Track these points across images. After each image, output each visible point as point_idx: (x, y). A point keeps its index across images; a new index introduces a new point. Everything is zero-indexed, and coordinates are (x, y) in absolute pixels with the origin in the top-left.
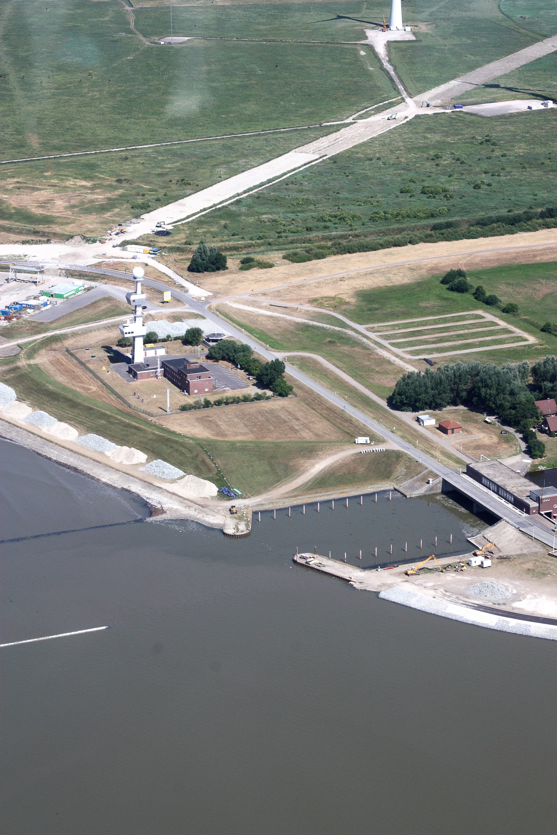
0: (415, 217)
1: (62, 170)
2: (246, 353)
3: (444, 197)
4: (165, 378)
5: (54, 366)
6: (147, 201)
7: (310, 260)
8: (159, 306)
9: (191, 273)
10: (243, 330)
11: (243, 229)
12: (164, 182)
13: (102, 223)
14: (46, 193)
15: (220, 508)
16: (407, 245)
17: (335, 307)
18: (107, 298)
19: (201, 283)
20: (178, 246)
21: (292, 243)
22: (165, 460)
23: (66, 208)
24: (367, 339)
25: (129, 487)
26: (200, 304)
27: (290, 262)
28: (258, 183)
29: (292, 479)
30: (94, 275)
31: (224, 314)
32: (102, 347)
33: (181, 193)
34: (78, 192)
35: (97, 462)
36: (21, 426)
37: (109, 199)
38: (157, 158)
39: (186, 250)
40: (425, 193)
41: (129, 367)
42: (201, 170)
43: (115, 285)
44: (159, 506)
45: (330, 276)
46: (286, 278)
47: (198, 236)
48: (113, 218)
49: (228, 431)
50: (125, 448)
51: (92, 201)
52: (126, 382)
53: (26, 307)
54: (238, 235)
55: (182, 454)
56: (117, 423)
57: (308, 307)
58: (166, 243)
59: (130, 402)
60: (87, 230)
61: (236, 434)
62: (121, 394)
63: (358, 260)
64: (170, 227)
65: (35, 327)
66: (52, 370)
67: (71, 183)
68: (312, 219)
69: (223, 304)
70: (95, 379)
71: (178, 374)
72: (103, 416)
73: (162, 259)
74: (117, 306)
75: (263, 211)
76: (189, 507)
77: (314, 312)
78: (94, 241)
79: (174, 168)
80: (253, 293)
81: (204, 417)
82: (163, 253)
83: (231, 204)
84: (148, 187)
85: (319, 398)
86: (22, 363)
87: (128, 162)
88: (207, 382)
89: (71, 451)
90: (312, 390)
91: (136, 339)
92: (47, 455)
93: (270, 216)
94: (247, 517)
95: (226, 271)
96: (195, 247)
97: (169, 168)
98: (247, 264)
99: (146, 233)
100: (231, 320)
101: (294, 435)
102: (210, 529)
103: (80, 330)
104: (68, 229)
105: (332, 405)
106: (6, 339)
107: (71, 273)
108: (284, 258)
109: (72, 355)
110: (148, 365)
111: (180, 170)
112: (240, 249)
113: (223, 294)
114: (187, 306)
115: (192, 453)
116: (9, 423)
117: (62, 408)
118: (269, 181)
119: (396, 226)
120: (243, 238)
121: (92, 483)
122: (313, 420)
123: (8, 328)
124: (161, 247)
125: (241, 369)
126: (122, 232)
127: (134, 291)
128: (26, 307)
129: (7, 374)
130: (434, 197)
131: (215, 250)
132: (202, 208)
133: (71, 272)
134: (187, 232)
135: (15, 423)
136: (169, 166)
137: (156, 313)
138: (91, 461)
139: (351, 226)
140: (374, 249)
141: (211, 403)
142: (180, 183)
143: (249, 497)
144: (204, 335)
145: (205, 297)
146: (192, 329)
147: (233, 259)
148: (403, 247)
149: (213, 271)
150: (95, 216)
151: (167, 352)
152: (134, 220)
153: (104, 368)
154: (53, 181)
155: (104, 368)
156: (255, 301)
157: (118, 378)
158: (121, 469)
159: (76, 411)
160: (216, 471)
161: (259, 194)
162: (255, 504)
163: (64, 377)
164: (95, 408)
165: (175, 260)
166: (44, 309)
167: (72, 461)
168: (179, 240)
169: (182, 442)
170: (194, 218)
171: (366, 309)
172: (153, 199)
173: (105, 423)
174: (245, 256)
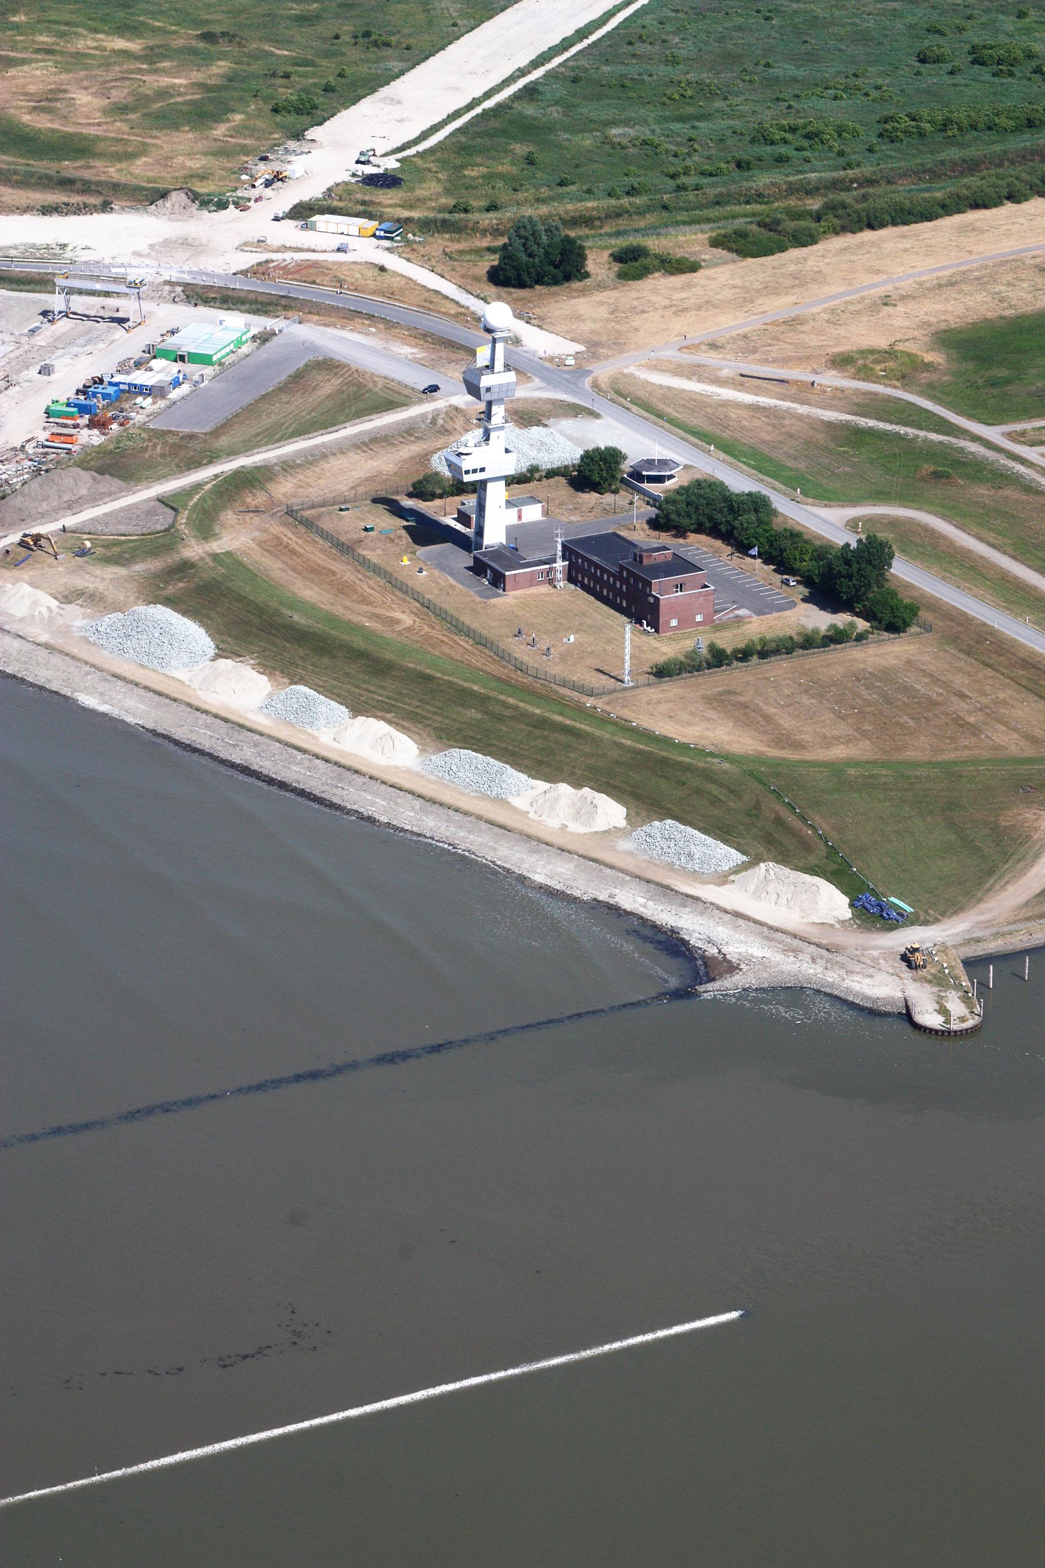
0: (990, 128)
3: (1035, 72)
4: (572, 587)
5: (276, 556)
7: (782, 249)
9: (500, 288)
11: (577, 166)
13: (215, 154)
15: (876, 953)
16: (1002, 204)
17: (904, 377)
19: (540, 318)
21: (717, 203)
23: (105, 112)
24: (1022, 464)
27: (734, 256)
28: (555, 40)
29: (1022, 864)
31: (649, 407)
34: (117, 68)
35: (500, 826)
36: (260, 728)
37: (203, 86)
40: (983, 64)
41: (475, 558)
43: (326, 325)
44: (713, 951)
45: (850, 293)
46: (745, 300)
47: (474, 188)
50: (564, 788)
51: (163, 93)
52: (478, 599)
53: (129, 392)
54: (573, 183)
55: (715, 801)
56: (512, 717)
57: (832, 379)
58: (402, 206)
61: (827, 742)
63: (901, 246)
64: (391, 163)
66: (274, 567)
67: (91, 43)
68: (736, 138)
69: (625, 376)
71: (618, 577)
72: (465, 697)
73: (409, 251)
76: (795, 951)
77: (857, 392)
78: (222, 205)
81: (720, 694)
82: (410, 236)
83: (516, 97)
84: (286, 53)
85: (991, 634)
86: (194, 550)
88: (701, 599)
90: (963, 614)
91: (489, 485)
92: (361, 810)
94: (955, 978)
95: (588, 282)
98: (633, 263)
99: (339, 181)
101: (974, 740)
102: (872, 1013)
103: (299, 453)
104: (140, 170)
105: (1033, 653)
106: (123, 484)
107: (199, 295)
108: (715, 243)
112: (597, 223)
115: (741, 798)
116: (226, 720)
118: (582, 33)
119: (952, 154)
122: (1001, 696)
123: (111, 452)
126: (278, 178)
128: (129, 392)
129: (167, 583)
130: (1011, 74)
132: (451, 111)
133: (199, 290)
134: (440, 175)
135: (241, 721)
138: (484, 826)
139: (841, 154)
140: (928, 216)
142: (360, 40)
143: (937, 921)
144: (626, 467)
148: (994, 211)
149: (556, 282)
150: (190, 135)
151: (546, 513)
152: (292, 145)
153: (406, 561)
154: (41, 38)
155: (406, 561)
156: (699, 366)
157: (451, 586)
160: (822, 851)
161: (573, 69)
162: (959, 939)
164: (438, 675)
166: (175, 394)
168: (431, 199)
169: (703, 770)
171: (980, 382)
172: (315, 85)
173: (479, 716)
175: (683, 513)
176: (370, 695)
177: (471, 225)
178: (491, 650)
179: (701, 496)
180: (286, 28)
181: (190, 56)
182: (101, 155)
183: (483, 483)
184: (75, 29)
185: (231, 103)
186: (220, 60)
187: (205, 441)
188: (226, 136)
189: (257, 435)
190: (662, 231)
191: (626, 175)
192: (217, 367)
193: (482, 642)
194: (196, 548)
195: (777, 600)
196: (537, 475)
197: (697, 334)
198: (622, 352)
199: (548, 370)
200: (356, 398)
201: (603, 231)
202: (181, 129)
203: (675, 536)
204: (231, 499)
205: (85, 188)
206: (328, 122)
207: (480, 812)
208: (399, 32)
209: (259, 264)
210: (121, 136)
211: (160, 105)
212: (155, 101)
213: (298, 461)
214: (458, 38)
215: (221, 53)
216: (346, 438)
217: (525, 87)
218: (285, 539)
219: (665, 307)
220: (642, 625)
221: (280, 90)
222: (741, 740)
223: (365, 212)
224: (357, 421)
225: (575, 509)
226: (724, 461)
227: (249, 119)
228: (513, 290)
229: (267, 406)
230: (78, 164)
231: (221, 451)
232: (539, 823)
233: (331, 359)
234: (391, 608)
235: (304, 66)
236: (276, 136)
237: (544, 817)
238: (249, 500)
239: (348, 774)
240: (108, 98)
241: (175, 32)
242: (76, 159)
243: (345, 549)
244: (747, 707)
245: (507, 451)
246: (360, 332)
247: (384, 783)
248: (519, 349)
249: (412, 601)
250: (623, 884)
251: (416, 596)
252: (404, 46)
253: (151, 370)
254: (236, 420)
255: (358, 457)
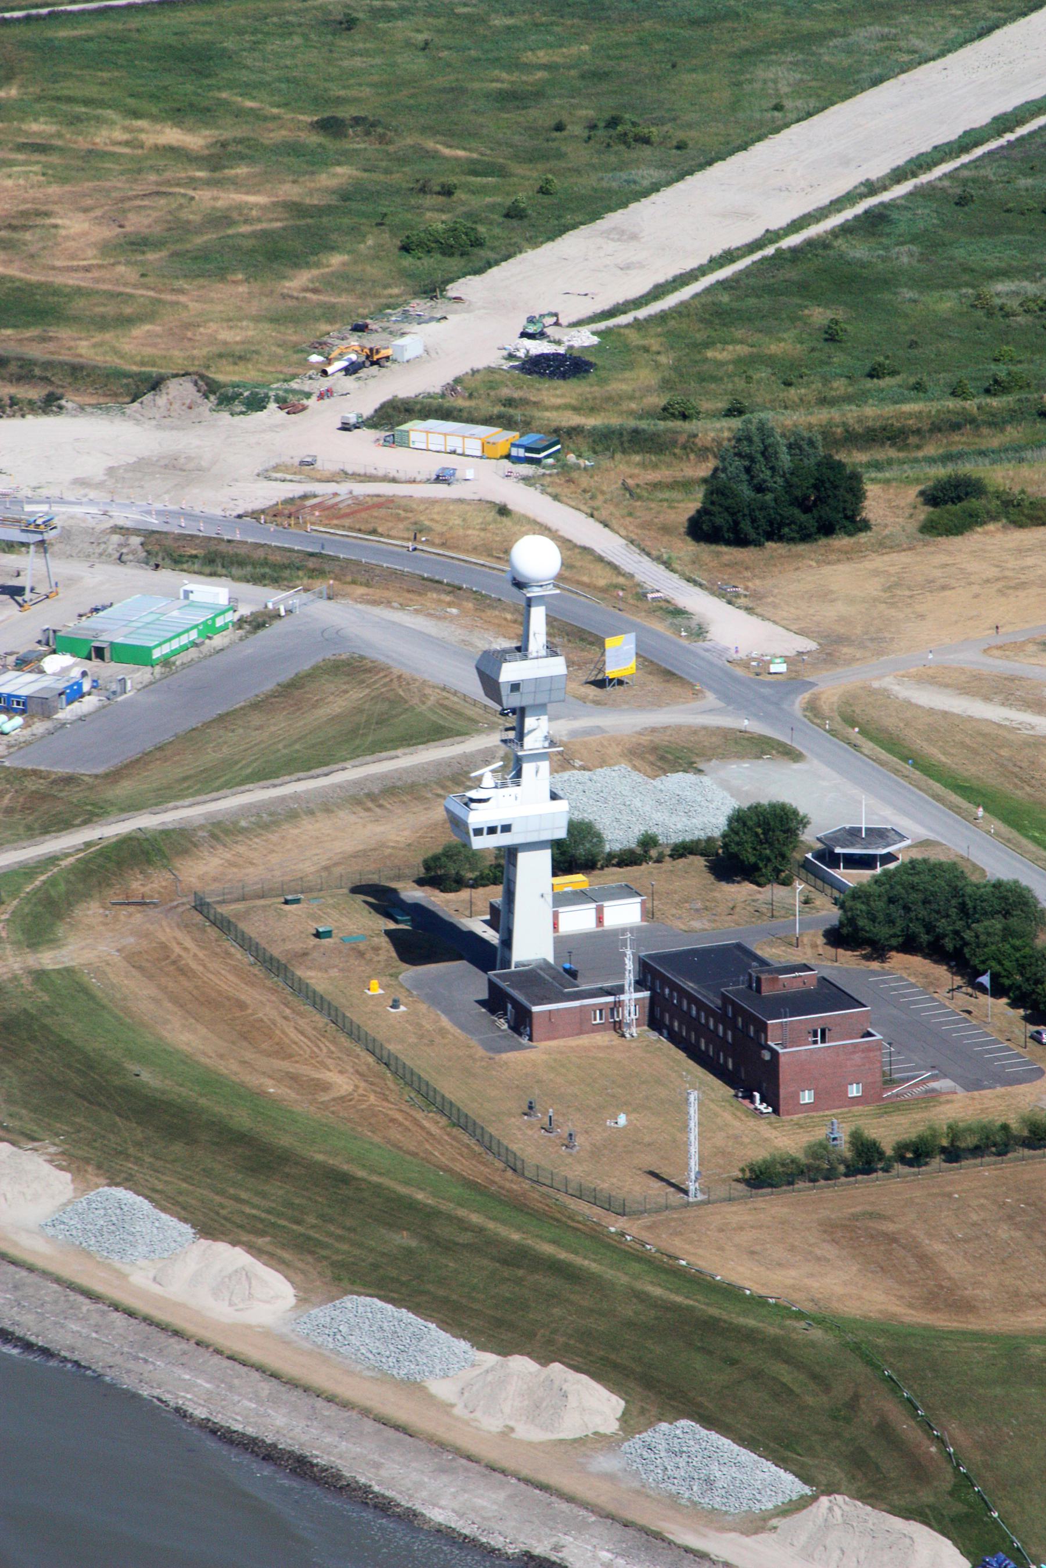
1: (66, 76)
2: (1013, 922)
4: (654, 1036)
5: (151, 977)
6: (469, 215)
8: (583, 699)
9: (703, 546)
10: (980, 812)
11: (913, 345)
12: (532, 130)
13: (276, 319)
14: (9, 183)
18: (347, 663)
19: (756, 596)
20: (632, 423)
22: (709, 1422)
23: (106, 248)
25: (556, 1548)
26: (766, 691)
28: (950, 133)
30: (277, 558)
31: (881, 738)
32: (356, 890)
33: (611, 181)
34: (153, 177)
35: (397, 1427)
36: (30, 1259)
37: (296, 209)
38: (483, 20)
39: (674, 443)
41: (491, 984)
42: (688, 78)
43: (375, 603)
47: (714, 379)
48: (322, 298)
49: (976, 1284)
50: (522, 1365)
51: (221, 219)
52: (481, 1052)
54: (894, 373)
55: (782, 1393)
58: (576, 409)
59: (514, 1147)
60: (215, 349)
61: (1016, 1302)
62: (472, 1109)
64: (584, 338)
65: (43, 797)
66: (139, 995)
67: (119, 135)
69: (872, 692)
70: (344, 1040)
71: (721, 1017)
72: (398, 1211)
74: (396, 701)
75: (992, 263)
78: (257, 404)
79: (570, 67)
80: (999, 641)
81: (855, 1217)
82: (572, 458)
83: (845, 230)
84: (461, 153)
87: (357, 41)
88: (857, 1058)
89: (275, 1376)
91: (522, 857)
93: (1030, 288)
95: (863, 537)
96: (716, 430)
97: (545, 67)
98: (954, 507)
99: (480, 365)
100: (916, 765)
103: (245, 810)
104: (133, 347)
107: (170, 551)
109: (224, 925)
110: (573, 974)
111: (598, 76)
112: (913, 440)
113: (862, 646)
114: (711, 699)
115: (827, 1389)
117: (207, 1172)
118: (1003, 123)
120: (918, 387)
121: (381, 1528)
124: (556, 431)
125: (998, 990)
126: (373, 360)
127: (515, 644)
131: (811, 443)
132: (716, 252)
133: (168, 542)
134: (663, 359)
136: (542, 56)
137: (573, 733)
138: (369, 1425)
141: (881, 1154)
142: (601, 133)
144: (809, 836)
145: (787, 659)
146: (755, 809)
147: (887, 481)
149: (805, 537)
150: (242, 289)
151: (648, 913)
152: (419, 306)
153: (375, 989)
154: (35, 127)
155: (375, 989)
156: (1012, 679)
157: (442, 1032)
158: (505, 1464)
159: (277, 1189)
160: (947, 1480)
161: (965, 182)
163: (203, 1031)
164: (361, 1173)
165: (626, 487)
166: (67, 713)
167: (283, 1424)
168: (631, 398)
169: (776, 1339)
170: (686, 293)
172: (492, 208)
174: (941, 472)
175: (881, 917)
176: (239, 1206)
177: (682, 439)
178: (473, 1135)
179: (913, 887)
180: (475, 111)
181: (298, 157)
182: (75, 320)
183: (511, 853)
184: (99, 111)
185: (334, 236)
186: (339, 164)
187: (91, 788)
188: (306, 290)
189: (185, 779)
190: (1029, 454)
191: (996, 360)
192: (158, 669)
193: (460, 1121)
194: (11, 960)
195: (1012, 1066)
196: (654, 853)
197: (1027, 626)
198: (880, 653)
199: (736, 679)
200: (382, 721)
201: (920, 454)
202: (229, 277)
203: (867, 958)
204: (104, 883)
205: (23, 372)
206: (494, 270)
207: (368, 1404)
208: (674, 119)
209: (290, 501)
210: (121, 289)
211: (206, 238)
212: (199, 231)
213: (243, 823)
214: (777, 130)
215: (345, 153)
216: (340, 786)
217: (866, 212)
218: (177, 950)
219: (988, 581)
220: (753, 1102)
221: (429, 214)
222: (865, 1294)
223: (500, 416)
224: (369, 758)
225: (706, 909)
226: (997, 834)
227: (355, 262)
228: (724, 549)
229: (221, 732)
230: (29, 333)
231: (112, 804)
232: (467, 1423)
233: (362, 658)
234: (322, 1063)
235: (485, 174)
236: (395, 291)
237: (477, 1415)
238: (135, 885)
239: (162, 1336)
240: (121, 226)
241: (275, 118)
242: (27, 325)
243: (274, 967)
244: (895, 1240)
245: (554, 797)
246: (430, 615)
247: (218, 1352)
248: (698, 646)
249: (364, 1054)
250: (582, 1527)
251: (370, 1047)
252: (675, 143)
253: (42, 672)
254: (158, 754)
255: (353, 818)
